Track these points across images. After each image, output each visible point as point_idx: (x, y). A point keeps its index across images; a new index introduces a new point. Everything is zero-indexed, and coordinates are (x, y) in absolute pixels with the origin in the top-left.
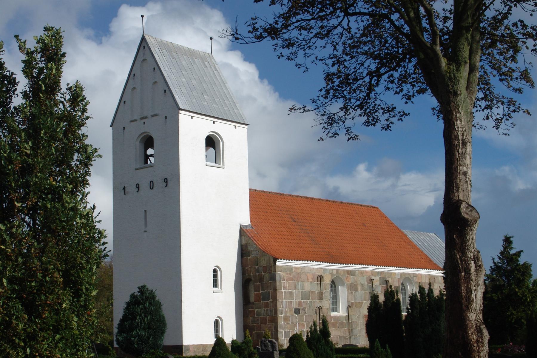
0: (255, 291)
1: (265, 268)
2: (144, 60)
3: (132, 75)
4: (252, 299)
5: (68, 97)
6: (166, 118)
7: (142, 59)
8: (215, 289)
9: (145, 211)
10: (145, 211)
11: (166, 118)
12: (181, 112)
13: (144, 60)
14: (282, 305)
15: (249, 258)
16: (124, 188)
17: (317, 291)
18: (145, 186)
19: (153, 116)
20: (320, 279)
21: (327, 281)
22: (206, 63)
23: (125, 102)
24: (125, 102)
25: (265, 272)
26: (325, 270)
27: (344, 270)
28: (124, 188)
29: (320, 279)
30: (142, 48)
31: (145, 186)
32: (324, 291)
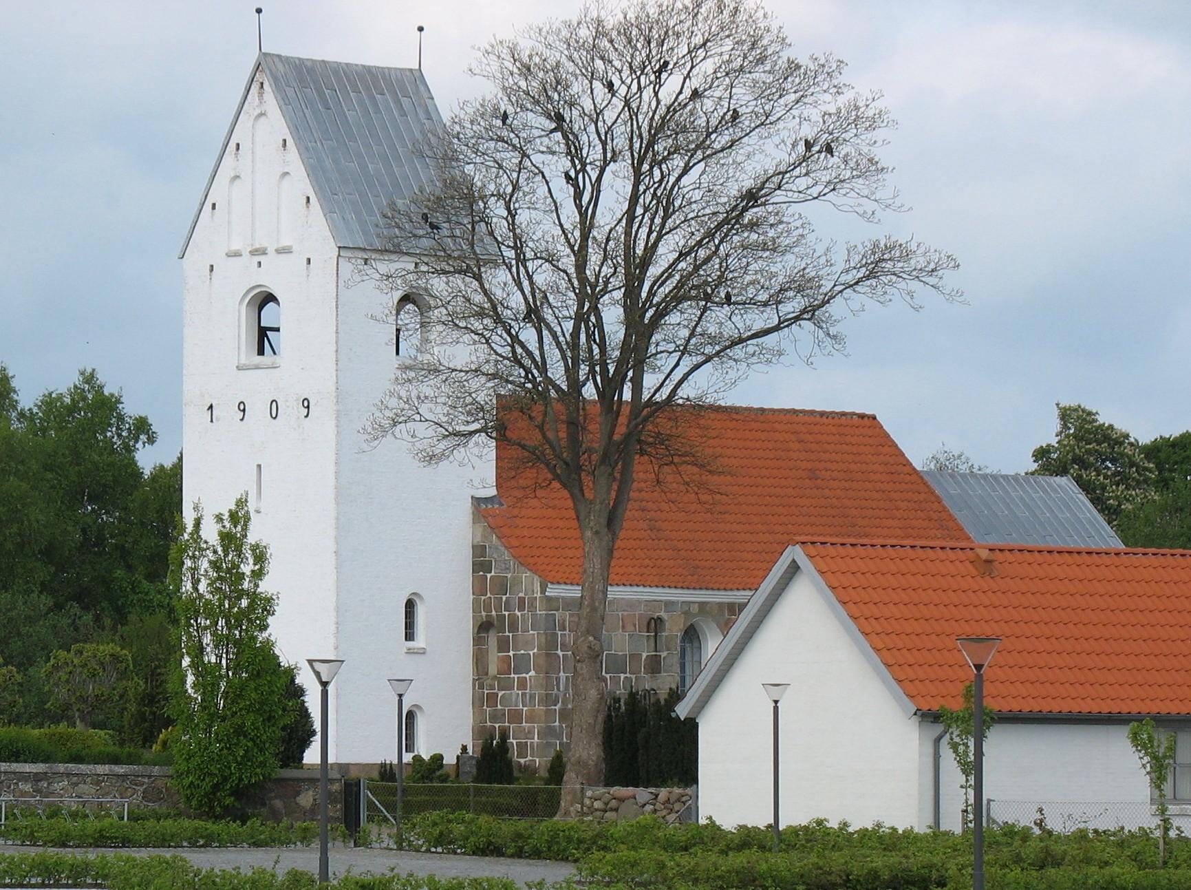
0: (500, 650)
1: (522, 600)
2: (262, 114)
3: (232, 145)
4: (493, 670)
5: (287, 721)
6: (309, 261)
7: (258, 111)
8: (410, 644)
9: (259, 466)
10: (259, 466)
11: (309, 261)
12: (331, 760)
13: (262, 114)
14: (558, 684)
15: (489, 576)
16: (211, 407)
17: (644, 655)
18: (257, 410)
19: (278, 251)
20: (655, 625)
21: (674, 629)
22: (404, 101)
23: (214, 206)
24: (214, 206)
25: (521, 608)
26: (669, 605)
27: (720, 605)
28: (211, 407)
29: (655, 625)
30: (255, 88)
31: (257, 410)
32: (664, 654)
